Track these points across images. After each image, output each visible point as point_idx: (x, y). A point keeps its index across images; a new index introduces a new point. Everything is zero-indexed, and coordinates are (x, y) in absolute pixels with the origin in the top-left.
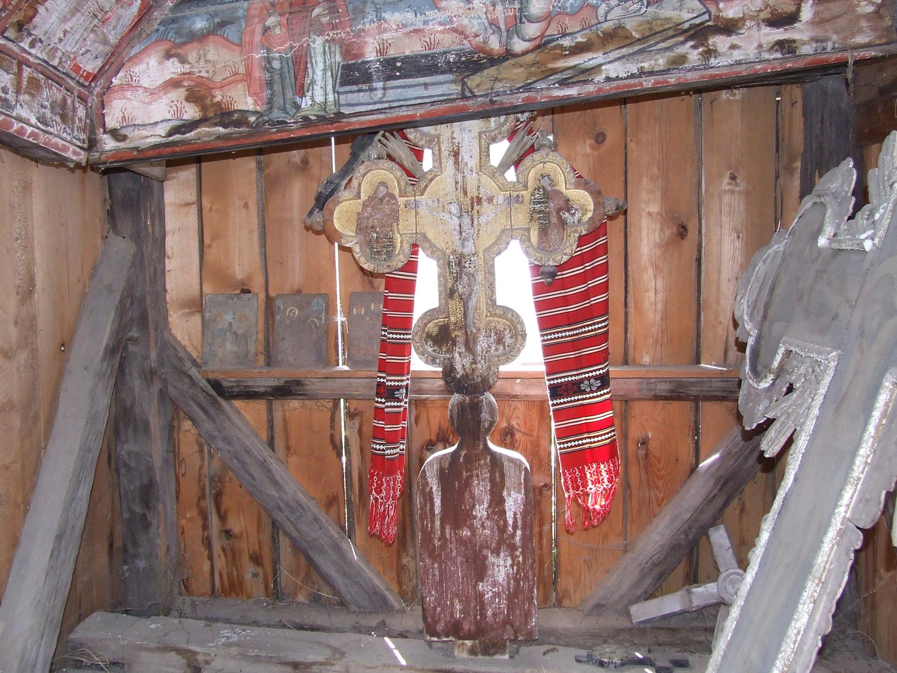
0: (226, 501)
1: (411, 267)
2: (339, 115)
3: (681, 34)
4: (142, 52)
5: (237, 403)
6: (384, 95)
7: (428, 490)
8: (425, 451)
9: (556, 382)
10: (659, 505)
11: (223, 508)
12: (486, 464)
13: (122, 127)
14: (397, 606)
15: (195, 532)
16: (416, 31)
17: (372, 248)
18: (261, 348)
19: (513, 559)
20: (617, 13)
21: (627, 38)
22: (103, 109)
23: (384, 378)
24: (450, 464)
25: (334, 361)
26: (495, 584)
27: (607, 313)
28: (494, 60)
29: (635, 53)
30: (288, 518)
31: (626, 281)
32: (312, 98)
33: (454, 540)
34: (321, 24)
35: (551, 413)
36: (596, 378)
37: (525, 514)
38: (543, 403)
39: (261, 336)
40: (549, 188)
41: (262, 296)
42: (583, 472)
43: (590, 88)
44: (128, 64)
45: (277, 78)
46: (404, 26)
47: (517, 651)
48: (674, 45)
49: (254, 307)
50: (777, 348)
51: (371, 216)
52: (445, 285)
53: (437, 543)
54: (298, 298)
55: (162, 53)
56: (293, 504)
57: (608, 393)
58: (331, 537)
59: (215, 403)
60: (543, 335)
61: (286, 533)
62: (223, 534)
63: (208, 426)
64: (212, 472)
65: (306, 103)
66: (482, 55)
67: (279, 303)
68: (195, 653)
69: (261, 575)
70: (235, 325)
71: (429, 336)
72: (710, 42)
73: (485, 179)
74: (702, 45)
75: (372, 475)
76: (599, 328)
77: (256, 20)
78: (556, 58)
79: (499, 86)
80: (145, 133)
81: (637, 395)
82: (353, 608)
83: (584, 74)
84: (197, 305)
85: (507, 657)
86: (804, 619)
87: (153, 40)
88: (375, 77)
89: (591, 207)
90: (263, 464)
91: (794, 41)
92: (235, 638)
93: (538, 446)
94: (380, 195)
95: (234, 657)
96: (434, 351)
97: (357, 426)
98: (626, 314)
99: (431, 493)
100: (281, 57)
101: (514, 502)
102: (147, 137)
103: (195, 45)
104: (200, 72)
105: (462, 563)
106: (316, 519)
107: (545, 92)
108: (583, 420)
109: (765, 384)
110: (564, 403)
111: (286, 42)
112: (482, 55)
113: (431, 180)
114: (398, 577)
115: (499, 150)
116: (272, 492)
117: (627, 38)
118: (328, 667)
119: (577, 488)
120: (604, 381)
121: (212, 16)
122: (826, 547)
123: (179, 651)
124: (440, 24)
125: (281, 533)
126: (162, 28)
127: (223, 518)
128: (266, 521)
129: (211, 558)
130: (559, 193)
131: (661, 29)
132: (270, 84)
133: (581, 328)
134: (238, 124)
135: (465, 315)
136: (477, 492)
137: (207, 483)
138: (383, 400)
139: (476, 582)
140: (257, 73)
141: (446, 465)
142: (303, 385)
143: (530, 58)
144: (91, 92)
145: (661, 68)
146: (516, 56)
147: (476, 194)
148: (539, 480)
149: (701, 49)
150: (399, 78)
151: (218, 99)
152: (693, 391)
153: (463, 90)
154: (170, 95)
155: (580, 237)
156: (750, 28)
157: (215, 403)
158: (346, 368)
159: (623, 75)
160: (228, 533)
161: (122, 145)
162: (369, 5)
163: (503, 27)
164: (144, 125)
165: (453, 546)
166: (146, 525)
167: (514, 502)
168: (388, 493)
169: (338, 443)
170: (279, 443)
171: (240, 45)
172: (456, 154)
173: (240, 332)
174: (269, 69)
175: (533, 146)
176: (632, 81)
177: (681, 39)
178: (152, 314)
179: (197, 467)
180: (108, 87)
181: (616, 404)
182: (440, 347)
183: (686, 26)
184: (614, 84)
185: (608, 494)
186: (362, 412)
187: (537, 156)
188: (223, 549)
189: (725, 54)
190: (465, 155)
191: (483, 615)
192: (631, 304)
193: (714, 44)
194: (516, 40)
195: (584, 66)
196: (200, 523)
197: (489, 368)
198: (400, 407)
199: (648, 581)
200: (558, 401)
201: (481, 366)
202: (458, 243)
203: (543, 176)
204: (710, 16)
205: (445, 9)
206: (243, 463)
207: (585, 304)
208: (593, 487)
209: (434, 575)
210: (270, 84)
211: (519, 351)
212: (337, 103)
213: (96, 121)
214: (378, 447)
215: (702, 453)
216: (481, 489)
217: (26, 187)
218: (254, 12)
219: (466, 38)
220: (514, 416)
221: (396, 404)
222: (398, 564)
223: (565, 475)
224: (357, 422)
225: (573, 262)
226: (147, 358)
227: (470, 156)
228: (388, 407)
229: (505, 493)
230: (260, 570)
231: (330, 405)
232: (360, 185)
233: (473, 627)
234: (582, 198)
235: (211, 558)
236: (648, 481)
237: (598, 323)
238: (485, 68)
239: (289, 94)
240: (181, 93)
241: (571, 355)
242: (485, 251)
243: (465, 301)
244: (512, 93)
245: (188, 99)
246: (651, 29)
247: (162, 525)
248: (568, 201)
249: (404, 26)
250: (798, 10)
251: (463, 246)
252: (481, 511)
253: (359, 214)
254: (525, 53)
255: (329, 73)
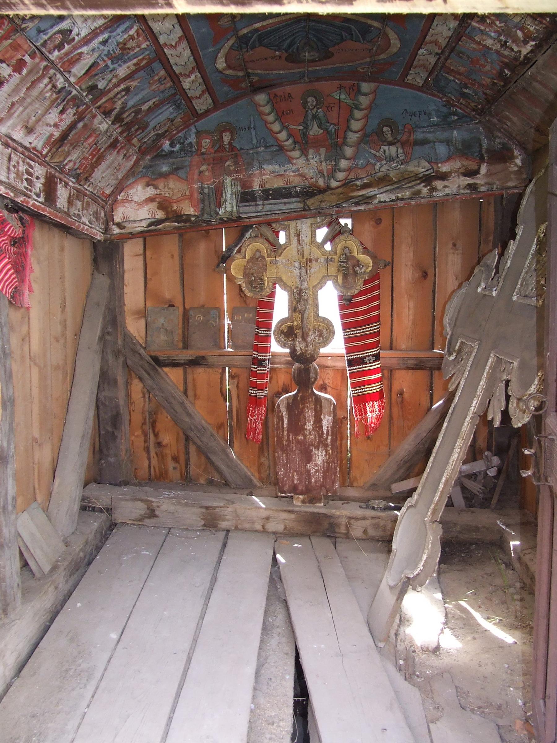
0: (159, 426)
1: (272, 295)
2: (239, 218)
3: (418, 180)
4: (133, 183)
5: (166, 369)
6: (263, 208)
7: (281, 414)
8: (275, 398)
9: (351, 357)
10: (409, 429)
11: (157, 430)
12: (312, 401)
13: (123, 222)
14: (258, 484)
15: (139, 442)
16: (280, 175)
17: (252, 285)
18: (181, 338)
19: (326, 452)
20: (385, 168)
21: (390, 181)
22: (113, 212)
23: (257, 354)
24: (293, 400)
25: (223, 347)
26: (316, 465)
27: (379, 321)
28: (321, 191)
29: (394, 189)
30: (196, 435)
31: (392, 302)
32: (225, 209)
33: (294, 441)
34: (230, 170)
35: (348, 375)
36: (373, 356)
37: (333, 428)
38: (343, 371)
39: (180, 332)
40: (348, 254)
41: (181, 309)
42: (365, 406)
43: (371, 206)
44: (126, 189)
45: (206, 198)
46: (274, 172)
47: (328, 503)
48: (414, 185)
49: (177, 315)
50: (458, 340)
51: (252, 267)
52: (292, 305)
53: (285, 443)
54: (203, 310)
55: (145, 183)
56: (199, 426)
57: (379, 364)
58: (221, 445)
59: (154, 369)
60: (344, 333)
61: (194, 443)
62: (156, 445)
63: (149, 382)
64: (150, 409)
65: (221, 211)
66: (314, 188)
67: (191, 312)
68: (153, 502)
69: (178, 469)
70: (166, 325)
71: (282, 332)
72: (433, 183)
73: (314, 249)
74: (429, 185)
75: (249, 407)
76: (375, 329)
77: (195, 167)
78: (353, 191)
79: (323, 205)
80: (135, 225)
81: (397, 367)
82: (233, 485)
83: (367, 199)
84: (143, 314)
85: (322, 504)
86: (456, 456)
87: (140, 176)
88: (258, 199)
89: (371, 264)
90: (182, 404)
91: (477, 184)
92: (172, 495)
93: (340, 395)
94: (257, 257)
95: (173, 504)
96: (285, 340)
97: (236, 383)
98: (392, 321)
99: (282, 416)
100: (209, 187)
101: (327, 421)
102: (136, 227)
103: (163, 179)
104: (165, 194)
105: (298, 454)
106: (212, 435)
107: (347, 208)
108: (365, 378)
109: (452, 358)
110: (355, 369)
111: (211, 179)
112: (314, 188)
113: (285, 249)
114: (259, 469)
115: (322, 233)
116: (187, 419)
117: (390, 181)
118: (225, 509)
119: (362, 415)
120: (377, 357)
121: (171, 164)
122: (466, 424)
123: (142, 501)
124: (293, 172)
125: (191, 443)
126: (144, 170)
127: (156, 435)
128: (182, 435)
129: (149, 458)
130: (354, 257)
131: (408, 176)
132: (203, 201)
133: (365, 329)
134: (185, 221)
135: (302, 321)
136: (307, 415)
137: (147, 415)
138: (256, 367)
139: (306, 464)
140: (196, 195)
141: (291, 401)
142: (206, 359)
143: (340, 190)
144: (107, 204)
145: (408, 197)
146: (332, 189)
147: (308, 257)
148: (340, 414)
149: (428, 188)
150: (270, 199)
151: (175, 208)
152: (429, 365)
153: (304, 206)
154: (149, 206)
155: (364, 281)
156: (454, 177)
157: (154, 369)
158: (230, 350)
159: (388, 200)
160: (159, 444)
161: (123, 231)
162: (255, 161)
163: (326, 174)
164: (135, 221)
165: (294, 445)
166: (114, 437)
167: (327, 421)
168: (258, 417)
169: (224, 391)
170: (190, 393)
171: (186, 180)
172: (298, 235)
173: (169, 329)
174: (202, 193)
175: (340, 231)
176: (392, 203)
177: (418, 182)
178: (119, 319)
179: (142, 406)
180: (115, 201)
181: (386, 372)
182: (288, 338)
183: (421, 175)
184: (383, 204)
185: (378, 418)
186: (239, 375)
187: (342, 237)
188: (156, 454)
189: (441, 190)
190: (303, 236)
191: (310, 482)
192: (395, 316)
193: (435, 185)
194: (332, 181)
195: (367, 195)
196: (142, 438)
197: (315, 350)
198: (265, 370)
199: (402, 471)
200: (352, 368)
201: (310, 349)
202: (299, 283)
203: (345, 248)
204: (433, 170)
205: (295, 164)
206: (170, 403)
207: (368, 316)
208: (370, 414)
209: (283, 460)
210: (203, 201)
211: (331, 341)
212: (238, 212)
213: (109, 219)
214: (253, 392)
215: (434, 400)
216: (309, 414)
217: (62, 249)
218: (194, 163)
219: (306, 179)
220: (327, 378)
221: (263, 369)
222: (258, 462)
223: (355, 408)
224: (236, 381)
225: (361, 293)
226: (116, 343)
227: (305, 237)
228: (259, 370)
229: (322, 416)
230: (177, 465)
231: (220, 371)
232: (246, 251)
233: (304, 488)
234: (366, 259)
235: (149, 458)
236: (403, 415)
237: (374, 326)
238: (316, 195)
239: (213, 207)
240: (155, 204)
241: (359, 343)
242: (313, 287)
243: (302, 314)
244: (330, 208)
245: (159, 208)
246: (403, 176)
247: (124, 438)
248: (358, 261)
249: (274, 172)
250: (479, 168)
251: (302, 284)
252: (309, 426)
253: (245, 266)
254: (337, 188)
255: (234, 196)
